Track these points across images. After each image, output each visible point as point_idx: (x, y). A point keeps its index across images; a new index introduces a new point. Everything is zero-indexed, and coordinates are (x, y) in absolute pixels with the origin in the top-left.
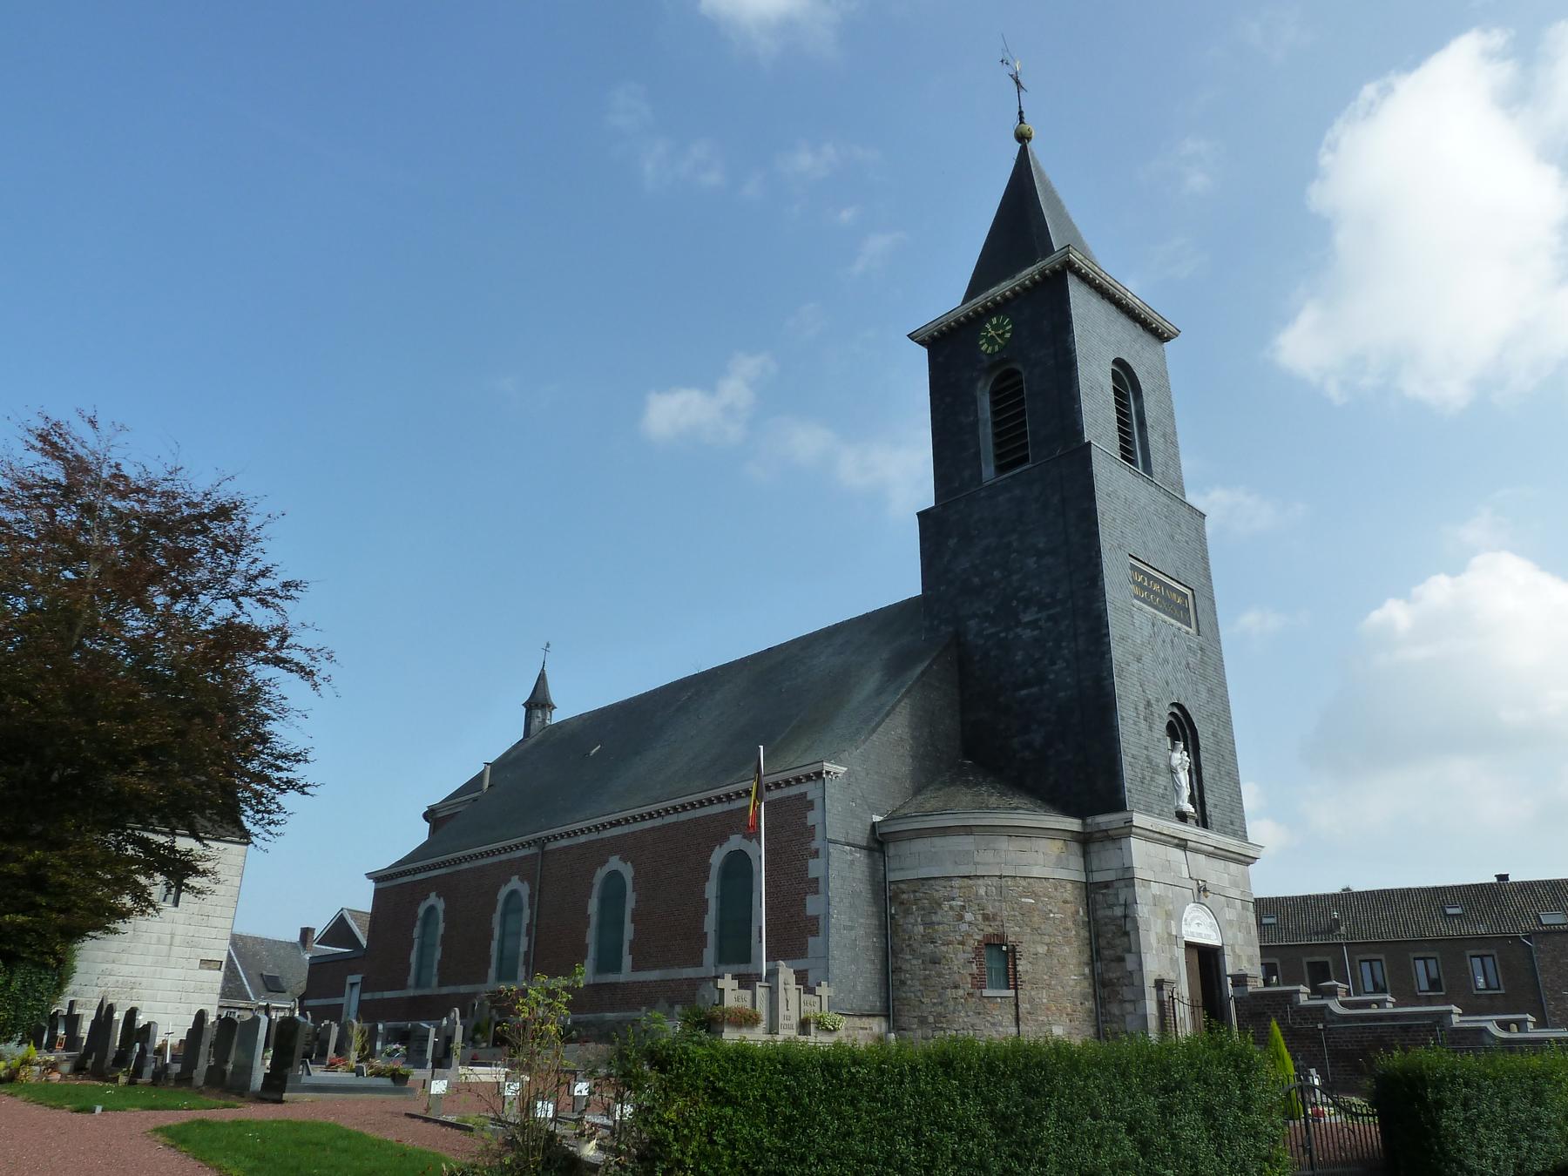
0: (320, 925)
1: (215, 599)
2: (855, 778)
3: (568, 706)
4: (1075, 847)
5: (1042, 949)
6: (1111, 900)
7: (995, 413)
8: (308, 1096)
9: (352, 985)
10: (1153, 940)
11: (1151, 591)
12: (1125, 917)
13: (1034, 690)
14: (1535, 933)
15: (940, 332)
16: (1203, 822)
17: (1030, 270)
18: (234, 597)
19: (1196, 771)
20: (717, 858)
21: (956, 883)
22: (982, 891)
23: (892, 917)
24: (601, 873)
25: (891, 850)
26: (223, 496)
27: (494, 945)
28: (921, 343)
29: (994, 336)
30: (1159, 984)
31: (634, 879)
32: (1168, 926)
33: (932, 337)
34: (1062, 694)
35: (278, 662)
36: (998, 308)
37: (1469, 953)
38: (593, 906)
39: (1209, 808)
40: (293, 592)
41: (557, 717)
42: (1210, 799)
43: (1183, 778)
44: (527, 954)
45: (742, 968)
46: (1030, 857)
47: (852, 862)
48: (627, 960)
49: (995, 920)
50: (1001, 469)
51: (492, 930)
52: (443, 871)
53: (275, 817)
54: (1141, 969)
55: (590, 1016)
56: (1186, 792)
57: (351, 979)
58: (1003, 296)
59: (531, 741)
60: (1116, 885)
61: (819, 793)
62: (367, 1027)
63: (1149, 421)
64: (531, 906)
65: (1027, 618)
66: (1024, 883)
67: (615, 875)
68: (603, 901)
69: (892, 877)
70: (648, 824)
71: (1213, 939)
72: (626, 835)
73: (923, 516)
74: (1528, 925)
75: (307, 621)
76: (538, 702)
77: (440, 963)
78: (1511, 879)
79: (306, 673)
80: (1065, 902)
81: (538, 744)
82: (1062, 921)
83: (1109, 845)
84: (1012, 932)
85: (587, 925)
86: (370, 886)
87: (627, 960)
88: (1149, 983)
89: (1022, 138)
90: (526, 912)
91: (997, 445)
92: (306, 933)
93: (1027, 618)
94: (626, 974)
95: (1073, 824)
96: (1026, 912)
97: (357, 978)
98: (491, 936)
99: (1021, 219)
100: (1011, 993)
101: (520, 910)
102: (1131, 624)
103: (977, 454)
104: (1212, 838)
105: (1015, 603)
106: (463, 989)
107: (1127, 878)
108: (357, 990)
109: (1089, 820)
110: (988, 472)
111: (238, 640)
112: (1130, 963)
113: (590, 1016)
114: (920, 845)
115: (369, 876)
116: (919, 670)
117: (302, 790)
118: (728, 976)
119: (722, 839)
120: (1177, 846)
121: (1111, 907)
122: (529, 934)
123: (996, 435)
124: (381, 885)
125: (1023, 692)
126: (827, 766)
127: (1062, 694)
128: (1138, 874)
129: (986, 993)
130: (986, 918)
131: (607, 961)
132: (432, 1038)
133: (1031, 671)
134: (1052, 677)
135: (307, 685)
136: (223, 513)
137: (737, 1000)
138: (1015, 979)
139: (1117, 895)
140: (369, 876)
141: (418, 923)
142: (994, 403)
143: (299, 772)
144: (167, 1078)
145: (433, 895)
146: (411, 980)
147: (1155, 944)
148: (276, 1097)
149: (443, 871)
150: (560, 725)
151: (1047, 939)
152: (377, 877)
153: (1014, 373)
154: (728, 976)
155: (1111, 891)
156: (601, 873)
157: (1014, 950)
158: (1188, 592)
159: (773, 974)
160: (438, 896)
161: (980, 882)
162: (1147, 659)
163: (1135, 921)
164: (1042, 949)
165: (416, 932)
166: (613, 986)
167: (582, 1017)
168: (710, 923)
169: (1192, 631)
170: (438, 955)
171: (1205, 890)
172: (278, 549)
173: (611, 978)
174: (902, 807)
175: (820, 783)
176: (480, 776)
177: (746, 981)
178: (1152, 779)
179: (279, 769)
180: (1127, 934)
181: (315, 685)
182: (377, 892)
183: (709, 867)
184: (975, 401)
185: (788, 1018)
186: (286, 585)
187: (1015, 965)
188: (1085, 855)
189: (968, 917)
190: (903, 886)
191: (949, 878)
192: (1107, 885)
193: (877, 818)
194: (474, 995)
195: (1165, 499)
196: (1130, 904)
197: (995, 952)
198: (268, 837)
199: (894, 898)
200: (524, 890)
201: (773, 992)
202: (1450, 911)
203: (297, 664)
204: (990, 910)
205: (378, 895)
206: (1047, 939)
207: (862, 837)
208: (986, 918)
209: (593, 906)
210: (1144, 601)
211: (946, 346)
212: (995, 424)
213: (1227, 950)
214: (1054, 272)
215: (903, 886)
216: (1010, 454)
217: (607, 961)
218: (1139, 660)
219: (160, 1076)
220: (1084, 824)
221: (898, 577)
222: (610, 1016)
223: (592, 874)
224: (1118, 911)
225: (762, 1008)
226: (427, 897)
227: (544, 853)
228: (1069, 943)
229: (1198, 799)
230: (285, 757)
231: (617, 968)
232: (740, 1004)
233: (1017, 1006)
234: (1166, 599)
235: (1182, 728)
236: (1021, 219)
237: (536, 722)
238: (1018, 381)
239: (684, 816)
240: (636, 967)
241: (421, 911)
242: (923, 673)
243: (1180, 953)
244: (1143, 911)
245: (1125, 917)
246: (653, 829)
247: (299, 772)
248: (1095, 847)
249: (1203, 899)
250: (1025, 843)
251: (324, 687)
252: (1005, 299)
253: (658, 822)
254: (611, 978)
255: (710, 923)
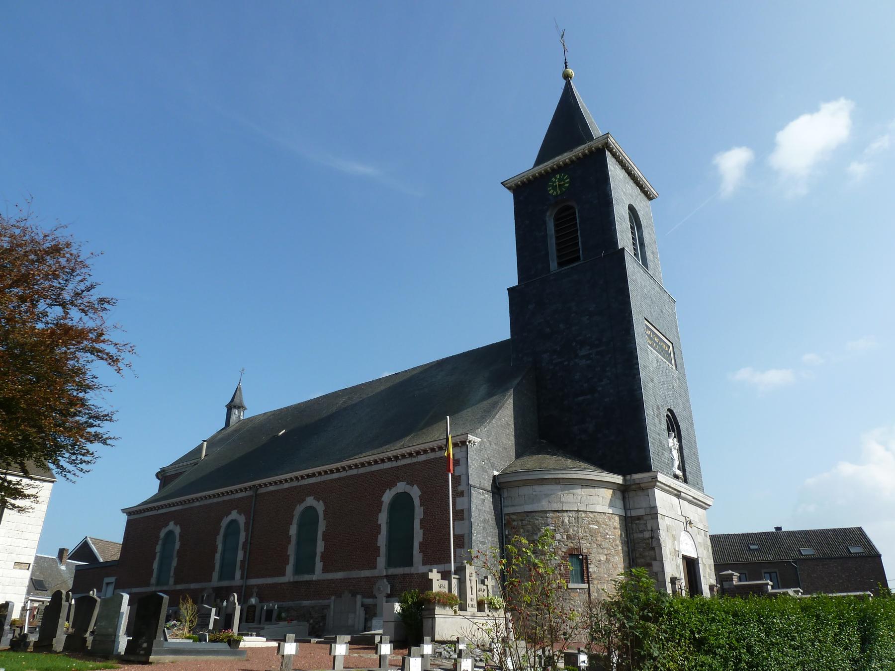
0: (72, 546)
1: (50, 305)
2: (488, 444)
3: (257, 406)
4: (619, 494)
5: (603, 558)
6: (641, 527)
7: (556, 231)
8: (169, 658)
9: (108, 584)
10: (668, 553)
11: (655, 342)
12: (652, 538)
13: (589, 396)
14: (799, 559)
15: (523, 183)
16: (685, 481)
17: (583, 146)
18: (63, 305)
19: (681, 450)
20: (387, 497)
21: (550, 515)
22: (566, 520)
23: (507, 537)
24: (300, 508)
25: (505, 494)
26: (62, 236)
27: (218, 556)
28: (509, 188)
29: (556, 187)
30: (673, 580)
31: (325, 511)
32: (674, 544)
33: (517, 186)
34: (607, 400)
35: (93, 351)
36: (554, 171)
37: (763, 571)
38: (293, 530)
39: (687, 474)
40: (106, 305)
41: (246, 415)
42: (688, 469)
43: (675, 454)
44: (242, 562)
45: (442, 567)
46: (591, 502)
47: (484, 500)
48: (319, 565)
49: (575, 539)
50: (560, 265)
51: (216, 547)
52: (180, 507)
53: (86, 458)
54: (663, 571)
55: (291, 603)
56: (676, 463)
57: (107, 580)
58: (564, 162)
59: (230, 429)
60: (645, 518)
61: (464, 454)
62: (196, 607)
63: (646, 243)
64: (246, 530)
65: (582, 353)
66: (591, 515)
67: (170, 533)
68: (300, 526)
69: (506, 510)
70: (336, 476)
71: (693, 555)
72: (320, 483)
73: (511, 291)
74: (794, 555)
75: (116, 325)
76: (233, 405)
77: (176, 568)
78: (783, 530)
79: (113, 360)
80: (615, 528)
81: (236, 431)
82: (614, 540)
83: (640, 493)
84: (585, 546)
85: (289, 542)
86: (124, 518)
87: (319, 565)
88: (668, 580)
89: (567, 77)
90: (243, 535)
91: (558, 250)
92: (62, 552)
93: (582, 353)
94: (318, 574)
95: (618, 479)
96: (594, 534)
97: (112, 579)
98: (215, 551)
99: (568, 122)
100: (585, 586)
101: (238, 533)
102: (649, 359)
103: (547, 255)
104: (693, 492)
105: (574, 344)
106: (193, 586)
107: (653, 513)
108: (111, 588)
109: (628, 477)
110: (553, 265)
111: (68, 334)
112: (656, 567)
113: (291, 603)
114: (526, 491)
115: (124, 511)
116: (516, 382)
117: (104, 442)
118: (435, 571)
119: (392, 484)
120: (676, 495)
121: (642, 532)
122: (244, 548)
123: (558, 244)
124: (132, 517)
125: (580, 398)
126: (471, 437)
127: (607, 400)
128: (660, 511)
129: (571, 586)
130: (569, 537)
131: (305, 565)
132: (213, 617)
133: (586, 385)
134: (600, 389)
135: (111, 370)
136: (56, 250)
137: (440, 587)
138: (588, 577)
139: (646, 524)
140: (124, 511)
141: (160, 542)
142: (556, 226)
143: (104, 428)
144: (27, 645)
145: (172, 523)
146: (153, 580)
147: (669, 556)
148: (143, 659)
149: (180, 507)
150: (250, 420)
151: (606, 552)
152: (129, 512)
153: (572, 208)
154: (435, 571)
155: (642, 522)
156: (300, 508)
157: (587, 559)
158: (670, 345)
159: (22, 615)
160: (176, 524)
161: (565, 514)
162: (656, 380)
163: (658, 540)
164: (603, 558)
165: (158, 548)
166: (309, 583)
167: (285, 604)
168: (382, 540)
169: (674, 367)
170: (174, 563)
171: (690, 523)
172: (104, 274)
173: (307, 577)
174: (510, 466)
175: (464, 449)
176: (200, 448)
177: (445, 576)
178: (663, 454)
179: (91, 426)
180: (653, 549)
181: (119, 370)
182: (128, 522)
183: (381, 503)
184: (545, 223)
185: (472, 600)
186: (102, 301)
187: (587, 568)
188: (624, 499)
189: (558, 536)
190: (514, 517)
191: (546, 512)
192: (639, 518)
193: (496, 473)
194: (203, 590)
195: (657, 288)
196: (655, 530)
197: (574, 560)
198: (78, 472)
199: (508, 523)
200: (242, 520)
201: (462, 583)
202: (752, 547)
203: (107, 354)
204: (571, 532)
205: (130, 525)
206: (606, 552)
207: (488, 485)
208: (569, 537)
209: (293, 530)
210: (651, 346)
211: (527, 194)
212: (557, 238)
213: (700, 560)
214: (598, 149)
215: (514, 517)
216: (567, 256)
217: (305, 565)
218: (652, 381)
219: (19, 644)
220: (624, 480)
221: (494, 326)
222: (306, 603)
223: (221, 519)
224: (647, 535)
225: (455, 591)
226: (167, 524)
227: (256, 495)
228: (617, 554)
229: (682, 467)
230: (97, 417)
231: (312, 571)
232: (442, 590)
233: (589, 593)
234: (660, 347)
235: (673, 425)
236: (568, 122)
237: (234, 418)
238: (569, 219)
239: (362, 471)
240: (325, 570)
241: (162, 534)
242: (518, 384)
243: (680, 561)
244: (663, 534)
245: (652, 538)
246: (339, 479)
247: (104, 428)
248: (631, 494)
249: (689, 529)
250: (592, 491)
251: (125, 371)
252: (566, 164)
253: (343, 474)
254: (307, 577)
255: (382, 540)
